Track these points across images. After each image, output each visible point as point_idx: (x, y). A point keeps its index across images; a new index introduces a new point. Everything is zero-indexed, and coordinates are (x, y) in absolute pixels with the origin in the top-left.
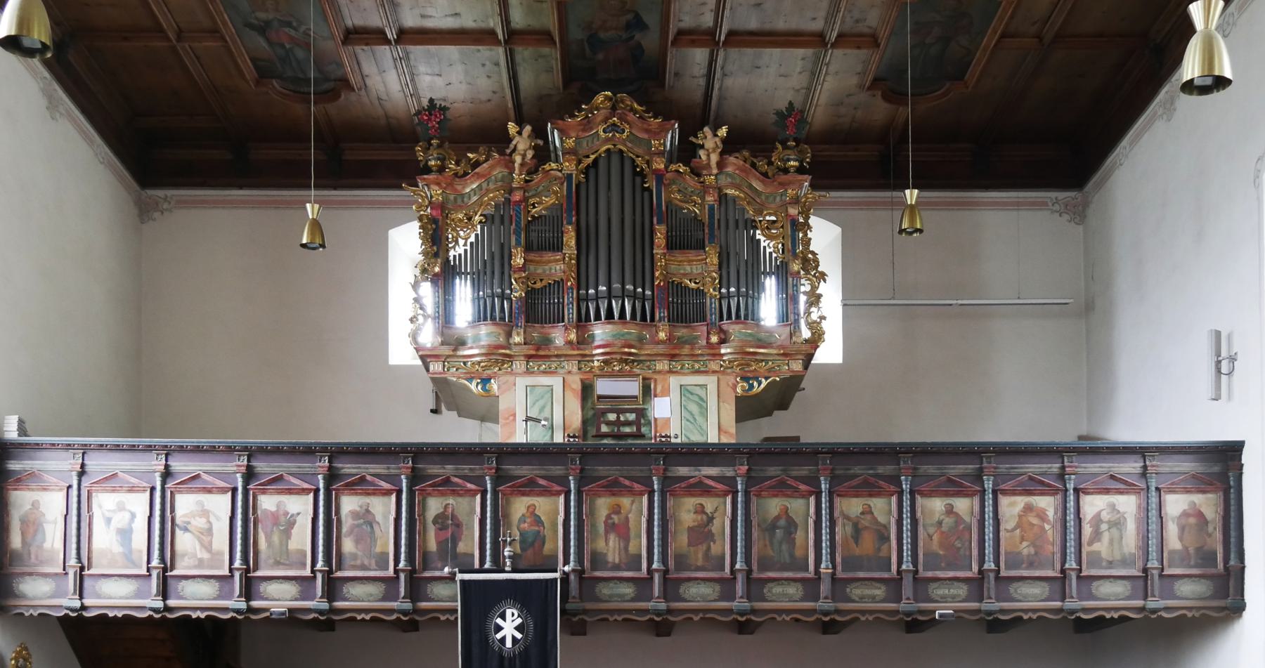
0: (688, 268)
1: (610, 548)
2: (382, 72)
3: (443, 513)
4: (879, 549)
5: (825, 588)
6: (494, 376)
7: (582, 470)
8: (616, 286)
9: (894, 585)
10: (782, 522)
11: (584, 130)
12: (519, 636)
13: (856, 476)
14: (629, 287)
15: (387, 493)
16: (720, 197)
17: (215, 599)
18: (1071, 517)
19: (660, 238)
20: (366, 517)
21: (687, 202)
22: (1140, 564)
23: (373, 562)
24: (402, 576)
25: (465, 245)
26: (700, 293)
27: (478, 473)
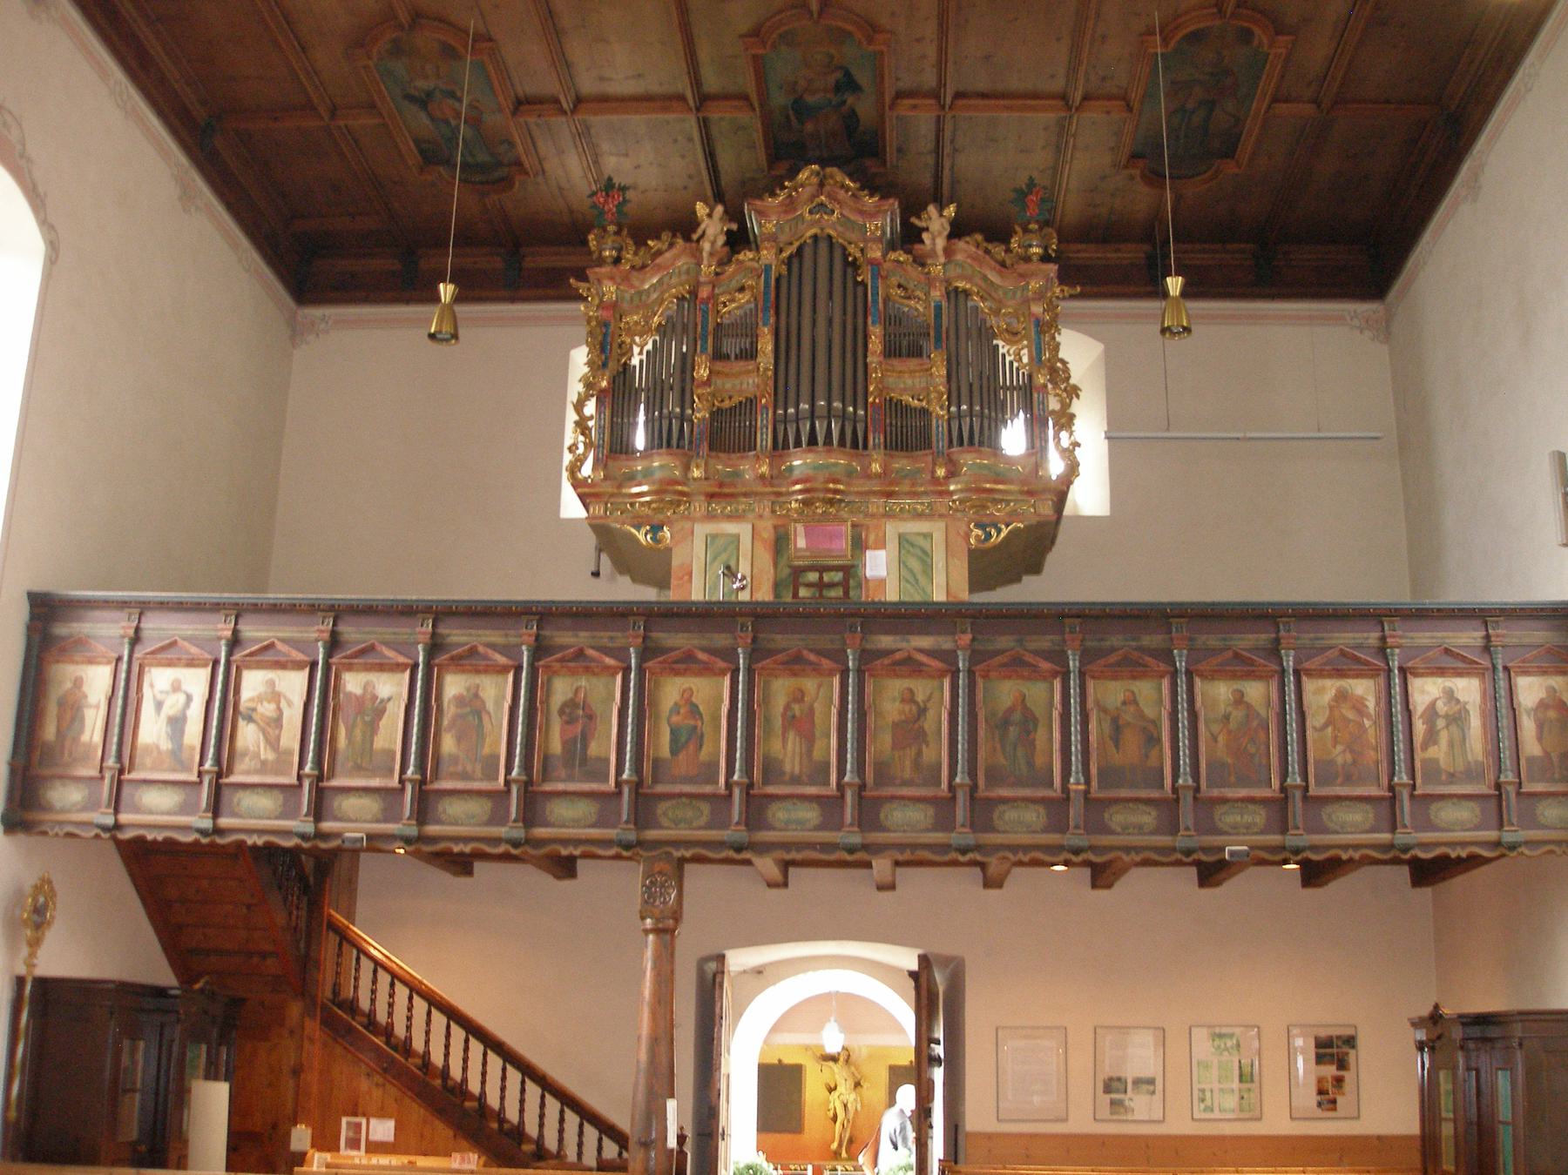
0: (909, 382)
1: (787, 750)
3: (572, 700)
5: (1075, 811)
6: (670, 523)
7: (754, 640)
9: (1169, 806)
10: (1017, 716)
11: (786, 212)
13: (1113, 650)
14: (837, 404)
15: (504, 670)
16: (948, 294)
17: (277, 818)
18: (1398, 708)
19: (876, 344)
20: (473, 704)
21: (909, 298)
22: (1490, 777)
23: (478, 767)
25: (641, 353)
26: (925, 413)
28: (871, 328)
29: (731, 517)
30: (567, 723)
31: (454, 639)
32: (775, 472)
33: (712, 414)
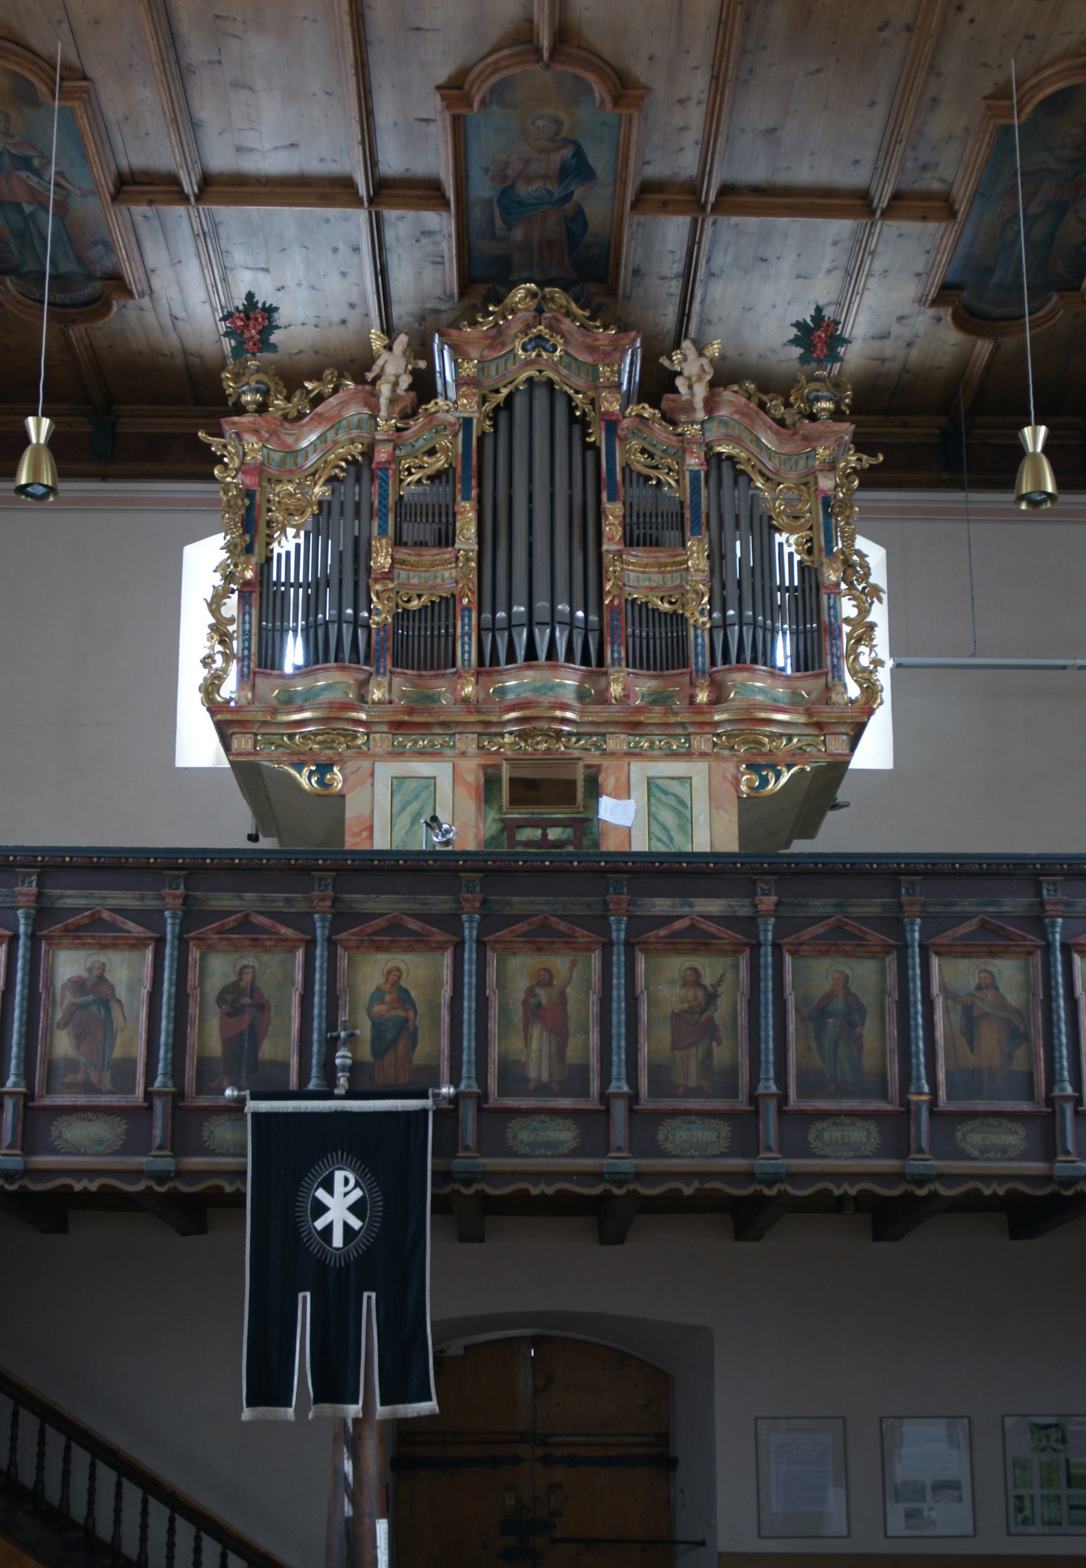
2: (176, 262)
3: (236, 984)
4: (1010, 1057)
6: (342, 762)
8: (542, 605)
10: (838, 1004)
11: (491, 347)
12: (356, 1223)
14: (563, 607)
15: (138, 944)
16: (708, 460)
20: (96, 990)
21: (656, 468)
23: (107, 1075)
24: (159, 1105)
27: (300, 907)
28: (607, 506)
29: (422, 754)
30: (230, 1015)
31: (69, 902)
32: (482, 696)
33: (396, 616)
